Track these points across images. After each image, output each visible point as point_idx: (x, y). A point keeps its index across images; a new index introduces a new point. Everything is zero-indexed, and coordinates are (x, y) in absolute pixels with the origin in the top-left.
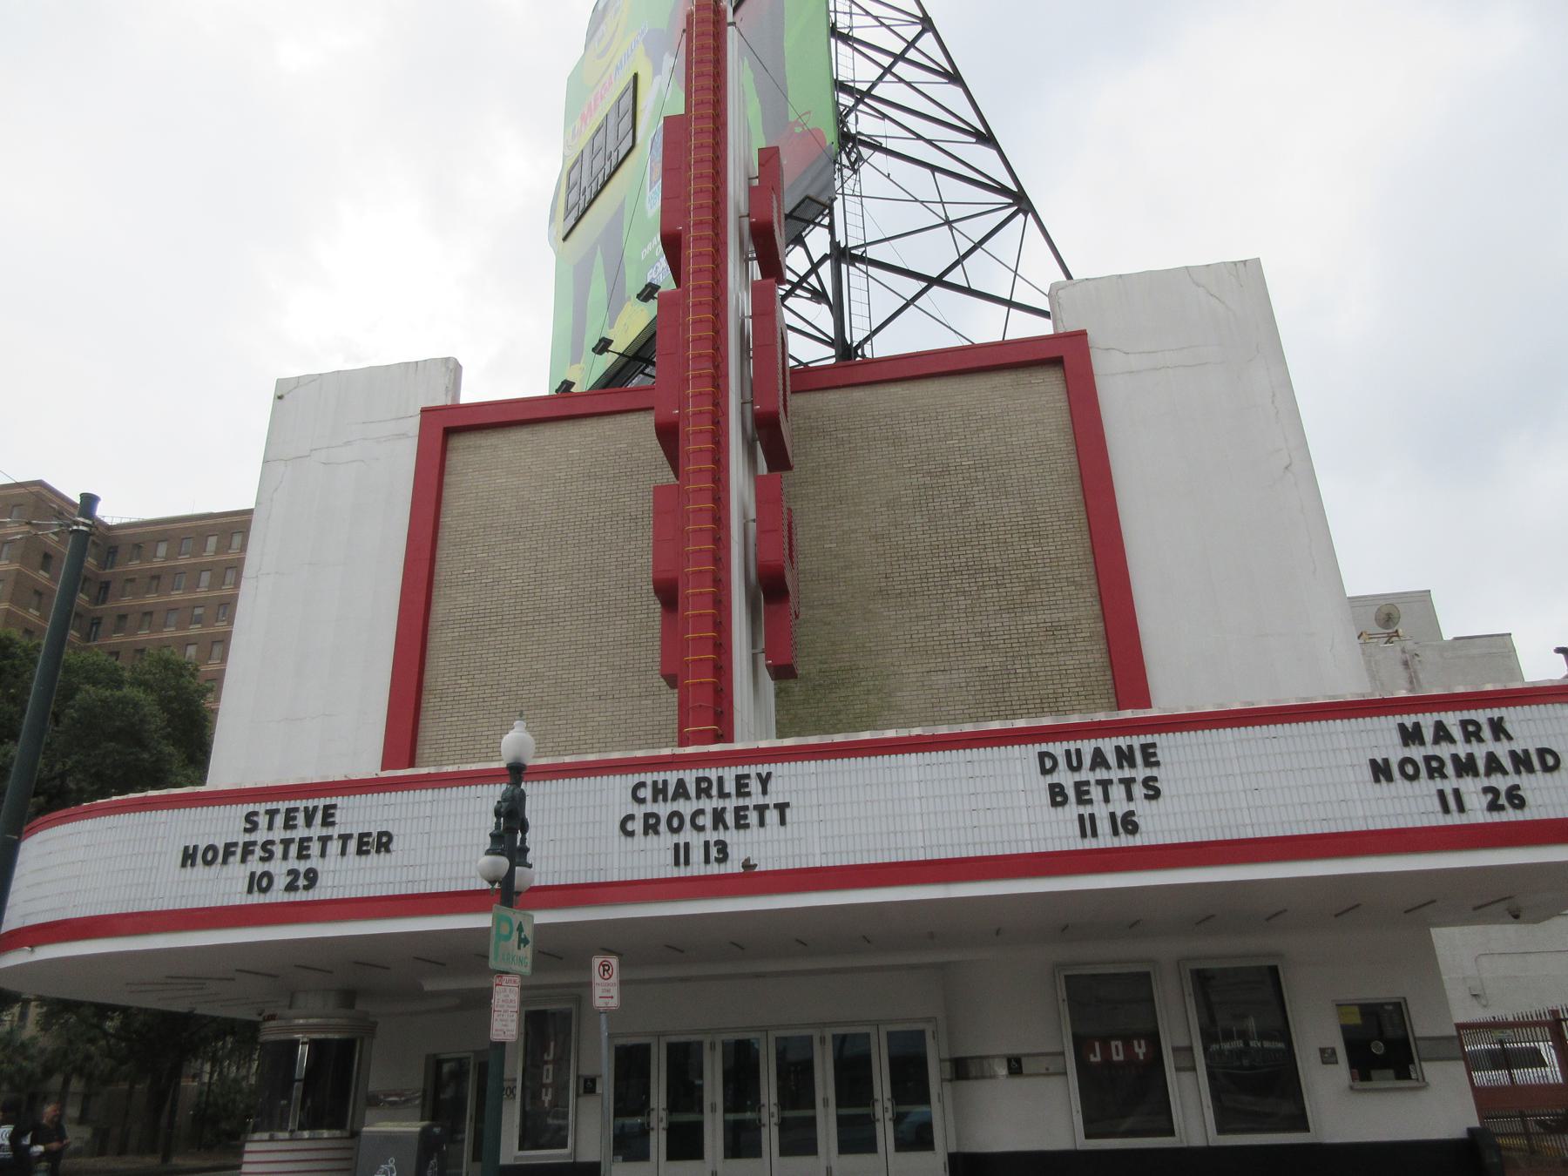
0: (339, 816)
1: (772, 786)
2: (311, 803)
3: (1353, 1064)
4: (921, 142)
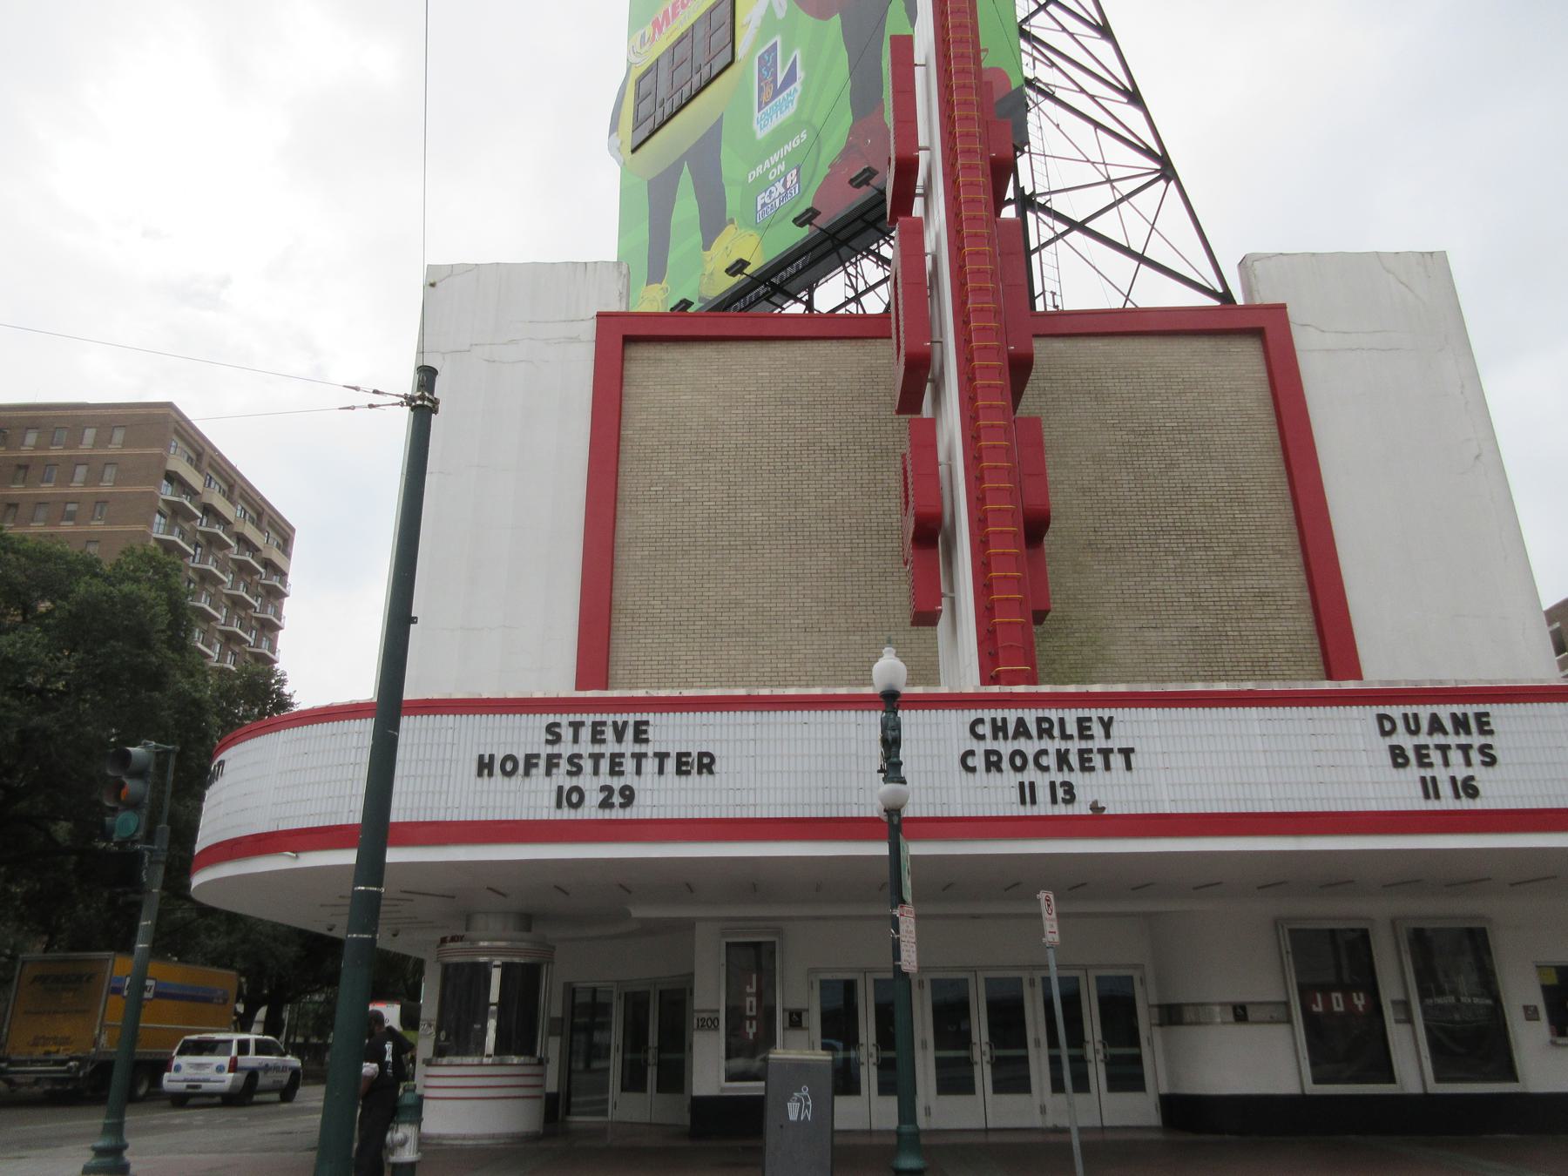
0: (651, 733)
1: (1114, 730)
2: (620, 718)
3: (1553, 1021)
4: (1083, 96)
